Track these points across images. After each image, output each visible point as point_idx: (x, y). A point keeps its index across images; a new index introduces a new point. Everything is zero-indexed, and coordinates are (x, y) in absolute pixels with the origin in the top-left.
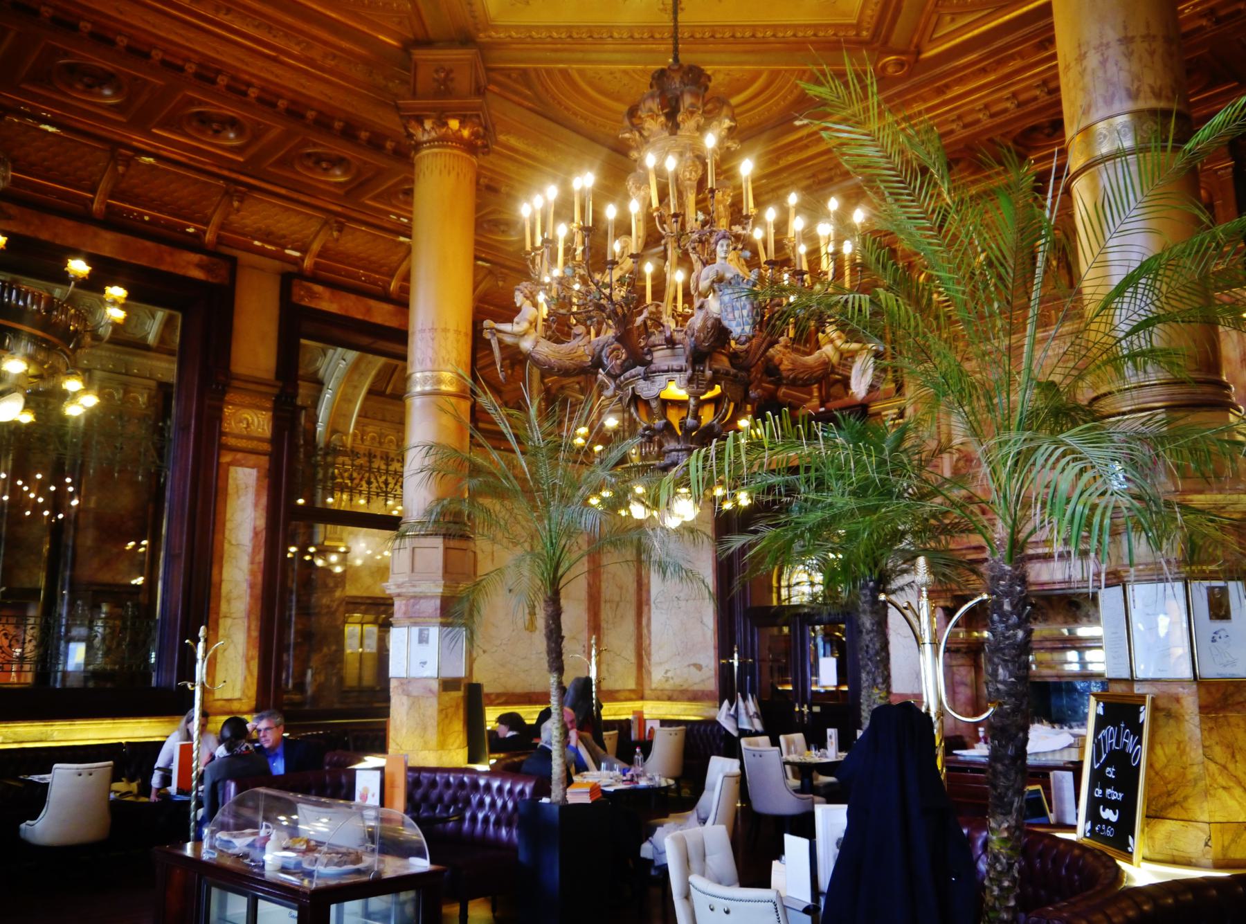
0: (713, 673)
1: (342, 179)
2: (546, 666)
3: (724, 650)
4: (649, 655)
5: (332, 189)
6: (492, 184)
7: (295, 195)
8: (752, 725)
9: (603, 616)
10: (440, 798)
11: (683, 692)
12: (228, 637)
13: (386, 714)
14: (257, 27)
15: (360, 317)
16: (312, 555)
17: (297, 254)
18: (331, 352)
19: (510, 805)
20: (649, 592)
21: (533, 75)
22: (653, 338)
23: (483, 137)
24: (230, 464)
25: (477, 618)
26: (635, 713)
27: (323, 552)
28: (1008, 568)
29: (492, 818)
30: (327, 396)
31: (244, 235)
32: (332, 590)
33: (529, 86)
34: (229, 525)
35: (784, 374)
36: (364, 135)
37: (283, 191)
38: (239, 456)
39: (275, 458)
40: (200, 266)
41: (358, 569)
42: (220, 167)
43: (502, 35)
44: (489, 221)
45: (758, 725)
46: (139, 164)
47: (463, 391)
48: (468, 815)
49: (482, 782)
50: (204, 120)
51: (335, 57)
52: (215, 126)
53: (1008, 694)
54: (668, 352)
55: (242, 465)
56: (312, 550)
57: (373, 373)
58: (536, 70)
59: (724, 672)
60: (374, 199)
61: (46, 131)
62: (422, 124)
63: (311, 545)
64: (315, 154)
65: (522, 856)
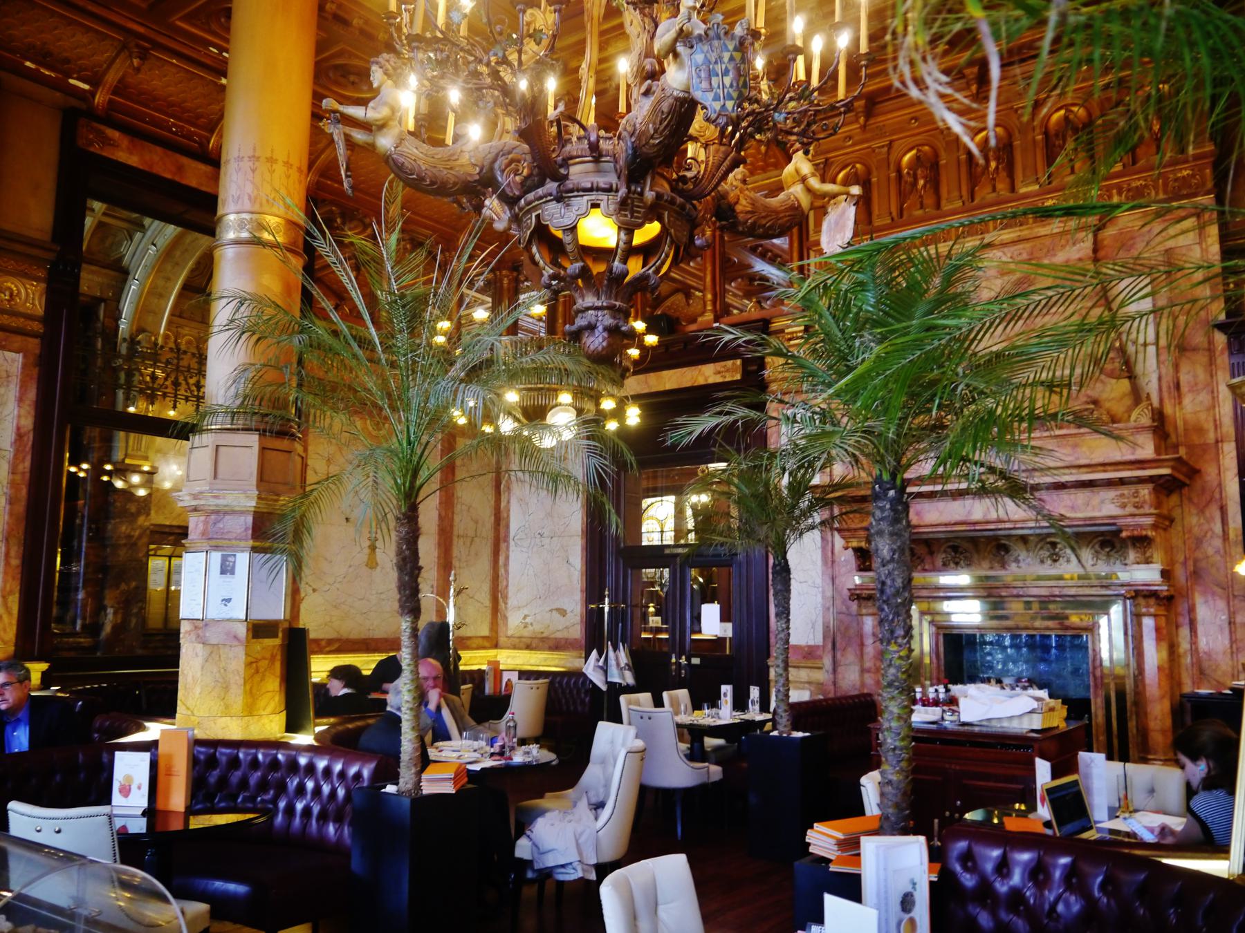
0: (578, 618)
2: (396, 605)
3: (593, 591)
4: (506, 598)
6: (341, 13)
8: (623, 677)
9: (455, 552)
10: (244, 783)
11: (543, 640)
13: (174, 661)
15: (168, 176)
16: (109, 473)
17: (86, 87)
19: (341, 792)
20: (508, 526)
22: (568, 147)
25: (307, 542)
26: (489, 663)
27: (122, 470)
29: (316, 809)
30: (133, 287)
32: (135, 516)
35: (741, 217)
39: (49, 341)
41: (166, 493)
44: (336, 67)
45: (629, 679)
47: (294, 243)
49: (303, 761)
54: (590, 166)
56: (108, 467)
57: (191, 264)
59: (593, 620)
60: (187, 18)
63: (109, 462)
65: (356, 863)
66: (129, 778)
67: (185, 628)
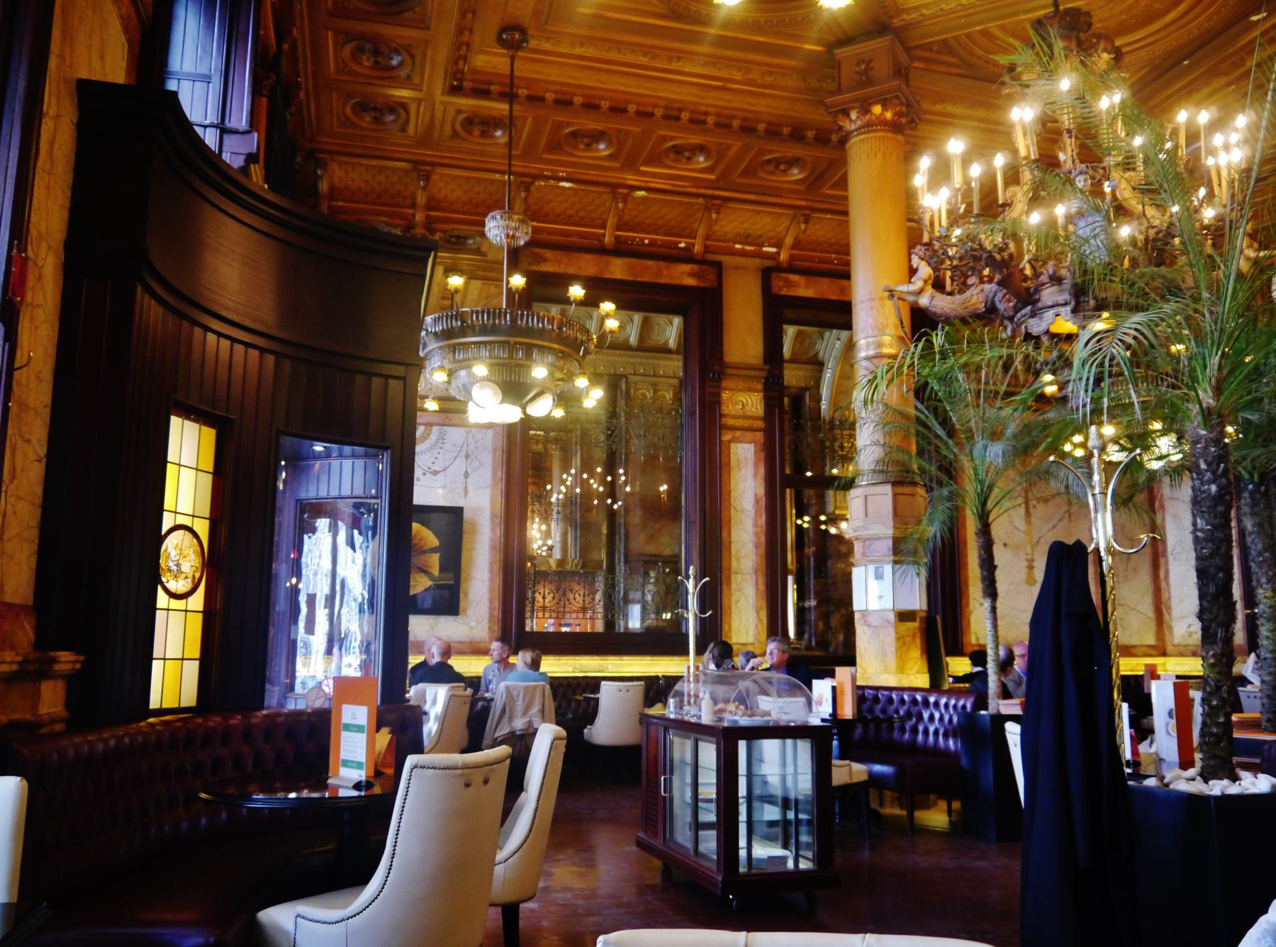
1: (801, 176)
4: (1169, 609)
5: (796, 187)
7: (764, 199)
12: (740, 590)
14: (704, 65)
16: (825, 523)
17: (774, 250)
18: (827, 334)
19: (955, 719)
21: (953, 43)
23: (907, 115)
24: (730, 441)
27: (834, 520)
28: (1203, 432)
29: (941, 732)
30: (828, 375)
31: (727, 241)
33: (951, 52)
34: (733, 494)
36: (810, 134)
37: (752, 197)
38: (738, 433)
39: (769, 432)
40: (692, 275)
42: (697, 187)
43: (914, 16)
46: (635, 198)
48: (921, 728)
50: (677, 150)
51: (771, 73)
52: (687, 154)
53: (1206, 540)
54: (1055, 288)
55: (741, 442)
56: (823, 518)
58: (955, 38)
60: (832, 187)
61: (564, 188)
62: (848, 115)
63: (824, 513)
64: (774, 159)
65: (964, 762)
66: (821, 695)
67: (857, 616)
